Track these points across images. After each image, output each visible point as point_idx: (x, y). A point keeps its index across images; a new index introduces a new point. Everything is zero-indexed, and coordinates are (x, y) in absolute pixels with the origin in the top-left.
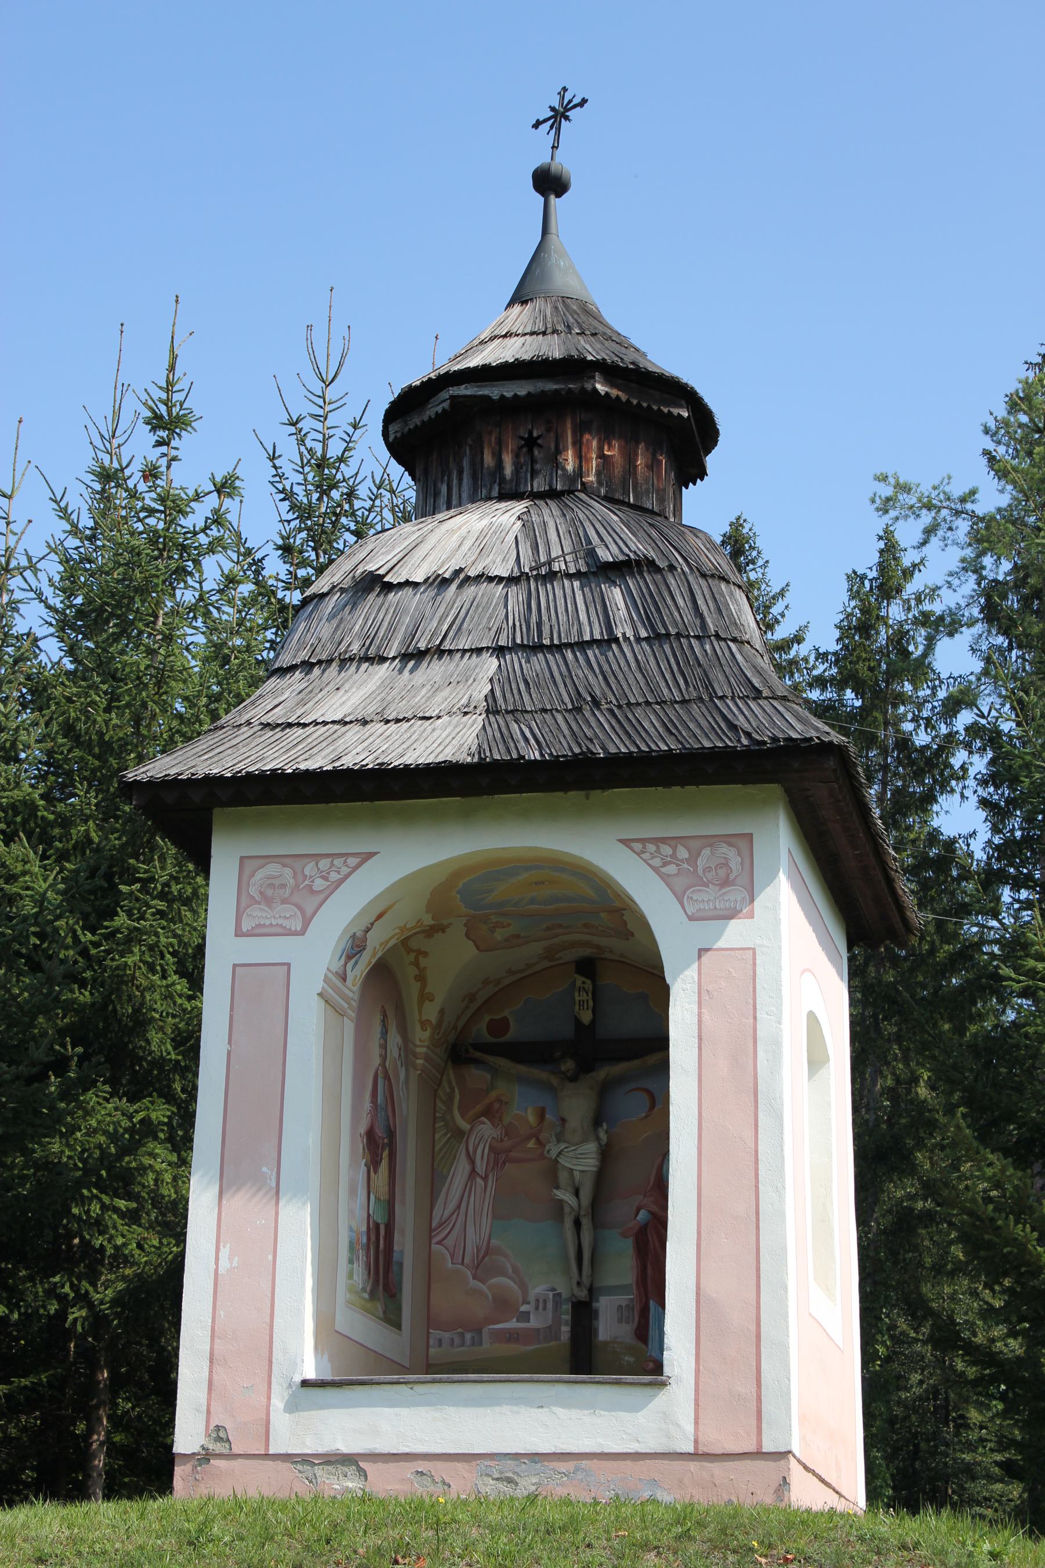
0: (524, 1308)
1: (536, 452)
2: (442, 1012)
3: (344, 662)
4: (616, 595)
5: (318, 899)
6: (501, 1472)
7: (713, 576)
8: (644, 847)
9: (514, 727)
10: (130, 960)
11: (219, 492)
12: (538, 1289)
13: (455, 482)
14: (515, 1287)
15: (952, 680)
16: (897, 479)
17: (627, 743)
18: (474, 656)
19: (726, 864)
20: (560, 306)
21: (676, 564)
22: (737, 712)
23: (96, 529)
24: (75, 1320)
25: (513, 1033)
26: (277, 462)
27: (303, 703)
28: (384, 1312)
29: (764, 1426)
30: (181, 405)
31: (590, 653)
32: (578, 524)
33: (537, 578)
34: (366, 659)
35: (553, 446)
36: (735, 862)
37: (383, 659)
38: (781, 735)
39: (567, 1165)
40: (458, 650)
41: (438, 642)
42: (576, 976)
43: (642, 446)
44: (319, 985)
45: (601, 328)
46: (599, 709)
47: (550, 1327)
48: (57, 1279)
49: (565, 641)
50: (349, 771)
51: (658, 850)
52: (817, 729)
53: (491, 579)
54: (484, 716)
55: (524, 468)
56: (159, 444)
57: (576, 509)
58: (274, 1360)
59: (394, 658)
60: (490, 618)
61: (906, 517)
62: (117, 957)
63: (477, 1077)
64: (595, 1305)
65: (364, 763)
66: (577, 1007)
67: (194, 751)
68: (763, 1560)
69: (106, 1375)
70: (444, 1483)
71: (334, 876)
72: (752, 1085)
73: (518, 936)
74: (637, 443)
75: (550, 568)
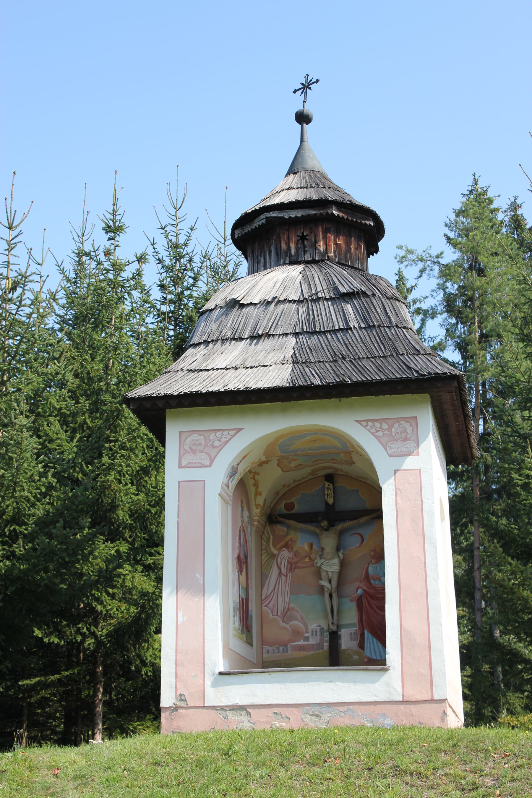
0: (306, 635)
1: (306, 242)
2: (265, 500)
3: (224, 341)
4: (349, 308)
5: (217, 450)
6: (313, 712)
7: (392, 298)
8: (367, 424)
9: (307, 370)
10: (111, 478)
11: (138, 261)
12: (313, 626)
13: (268, 257)
14: (302, 625)
15: (430, 339)
16: (407, 247)
17: (361, 376)
18: (284, 337)
19: (405, 431)
20: (312, 175)
21: (375, 293)
22: (410, 361)
23: (77, 278)
24: (89, 644)
25: (297, 509)
26: (155, 246)
27: (206, 360)
28: (247, 639)
29: (434, 688)
30: (120, 221)
31: (338, 335)
32: (328, 275)
33: (311, 300)
34: (234, 339)
35: (313, 239)
36: (409, 429)
37: (242, 339)
38: (432, 372)
39: (325, 569)
40: (277, 334)
41: (267, 331)
42: (325, 482)
43: (353, 239)
44: (219, 490)
45: (331, 185)
46: (345, 360)
47: (319, 643)
48: (80, 625)
49: (326, 329)
50: (232, 391)
51: (374, 425)
52: (448, 369)
53: (290, 301)
54: (292, 365)
55: (300, 250)
56: (110, 239)
57: (326, 269)
58: (205, 663)
59: (247, 338)
60: (291, 319)
61: (411, 265)
62: (103, 477)
63: (280, 529)
64: (339, 633)
65: (239, 387)
66: (326, 496)
67: (159, 382)
68: (495, 756)
69: (101, 669)
70: (287, 717)
71: (224, 440)
72: (422, 532)
73: (301, 465)
74: (351, 238)
75: (317, 296)
